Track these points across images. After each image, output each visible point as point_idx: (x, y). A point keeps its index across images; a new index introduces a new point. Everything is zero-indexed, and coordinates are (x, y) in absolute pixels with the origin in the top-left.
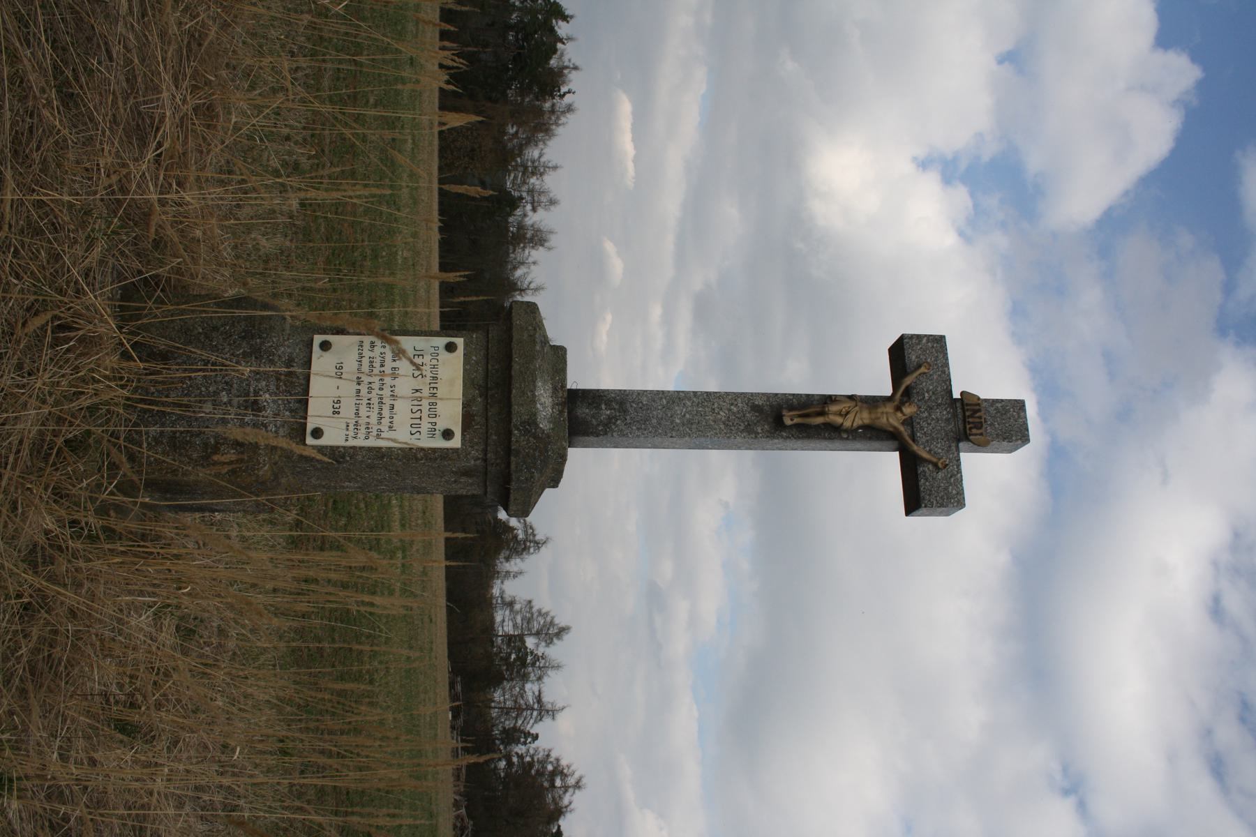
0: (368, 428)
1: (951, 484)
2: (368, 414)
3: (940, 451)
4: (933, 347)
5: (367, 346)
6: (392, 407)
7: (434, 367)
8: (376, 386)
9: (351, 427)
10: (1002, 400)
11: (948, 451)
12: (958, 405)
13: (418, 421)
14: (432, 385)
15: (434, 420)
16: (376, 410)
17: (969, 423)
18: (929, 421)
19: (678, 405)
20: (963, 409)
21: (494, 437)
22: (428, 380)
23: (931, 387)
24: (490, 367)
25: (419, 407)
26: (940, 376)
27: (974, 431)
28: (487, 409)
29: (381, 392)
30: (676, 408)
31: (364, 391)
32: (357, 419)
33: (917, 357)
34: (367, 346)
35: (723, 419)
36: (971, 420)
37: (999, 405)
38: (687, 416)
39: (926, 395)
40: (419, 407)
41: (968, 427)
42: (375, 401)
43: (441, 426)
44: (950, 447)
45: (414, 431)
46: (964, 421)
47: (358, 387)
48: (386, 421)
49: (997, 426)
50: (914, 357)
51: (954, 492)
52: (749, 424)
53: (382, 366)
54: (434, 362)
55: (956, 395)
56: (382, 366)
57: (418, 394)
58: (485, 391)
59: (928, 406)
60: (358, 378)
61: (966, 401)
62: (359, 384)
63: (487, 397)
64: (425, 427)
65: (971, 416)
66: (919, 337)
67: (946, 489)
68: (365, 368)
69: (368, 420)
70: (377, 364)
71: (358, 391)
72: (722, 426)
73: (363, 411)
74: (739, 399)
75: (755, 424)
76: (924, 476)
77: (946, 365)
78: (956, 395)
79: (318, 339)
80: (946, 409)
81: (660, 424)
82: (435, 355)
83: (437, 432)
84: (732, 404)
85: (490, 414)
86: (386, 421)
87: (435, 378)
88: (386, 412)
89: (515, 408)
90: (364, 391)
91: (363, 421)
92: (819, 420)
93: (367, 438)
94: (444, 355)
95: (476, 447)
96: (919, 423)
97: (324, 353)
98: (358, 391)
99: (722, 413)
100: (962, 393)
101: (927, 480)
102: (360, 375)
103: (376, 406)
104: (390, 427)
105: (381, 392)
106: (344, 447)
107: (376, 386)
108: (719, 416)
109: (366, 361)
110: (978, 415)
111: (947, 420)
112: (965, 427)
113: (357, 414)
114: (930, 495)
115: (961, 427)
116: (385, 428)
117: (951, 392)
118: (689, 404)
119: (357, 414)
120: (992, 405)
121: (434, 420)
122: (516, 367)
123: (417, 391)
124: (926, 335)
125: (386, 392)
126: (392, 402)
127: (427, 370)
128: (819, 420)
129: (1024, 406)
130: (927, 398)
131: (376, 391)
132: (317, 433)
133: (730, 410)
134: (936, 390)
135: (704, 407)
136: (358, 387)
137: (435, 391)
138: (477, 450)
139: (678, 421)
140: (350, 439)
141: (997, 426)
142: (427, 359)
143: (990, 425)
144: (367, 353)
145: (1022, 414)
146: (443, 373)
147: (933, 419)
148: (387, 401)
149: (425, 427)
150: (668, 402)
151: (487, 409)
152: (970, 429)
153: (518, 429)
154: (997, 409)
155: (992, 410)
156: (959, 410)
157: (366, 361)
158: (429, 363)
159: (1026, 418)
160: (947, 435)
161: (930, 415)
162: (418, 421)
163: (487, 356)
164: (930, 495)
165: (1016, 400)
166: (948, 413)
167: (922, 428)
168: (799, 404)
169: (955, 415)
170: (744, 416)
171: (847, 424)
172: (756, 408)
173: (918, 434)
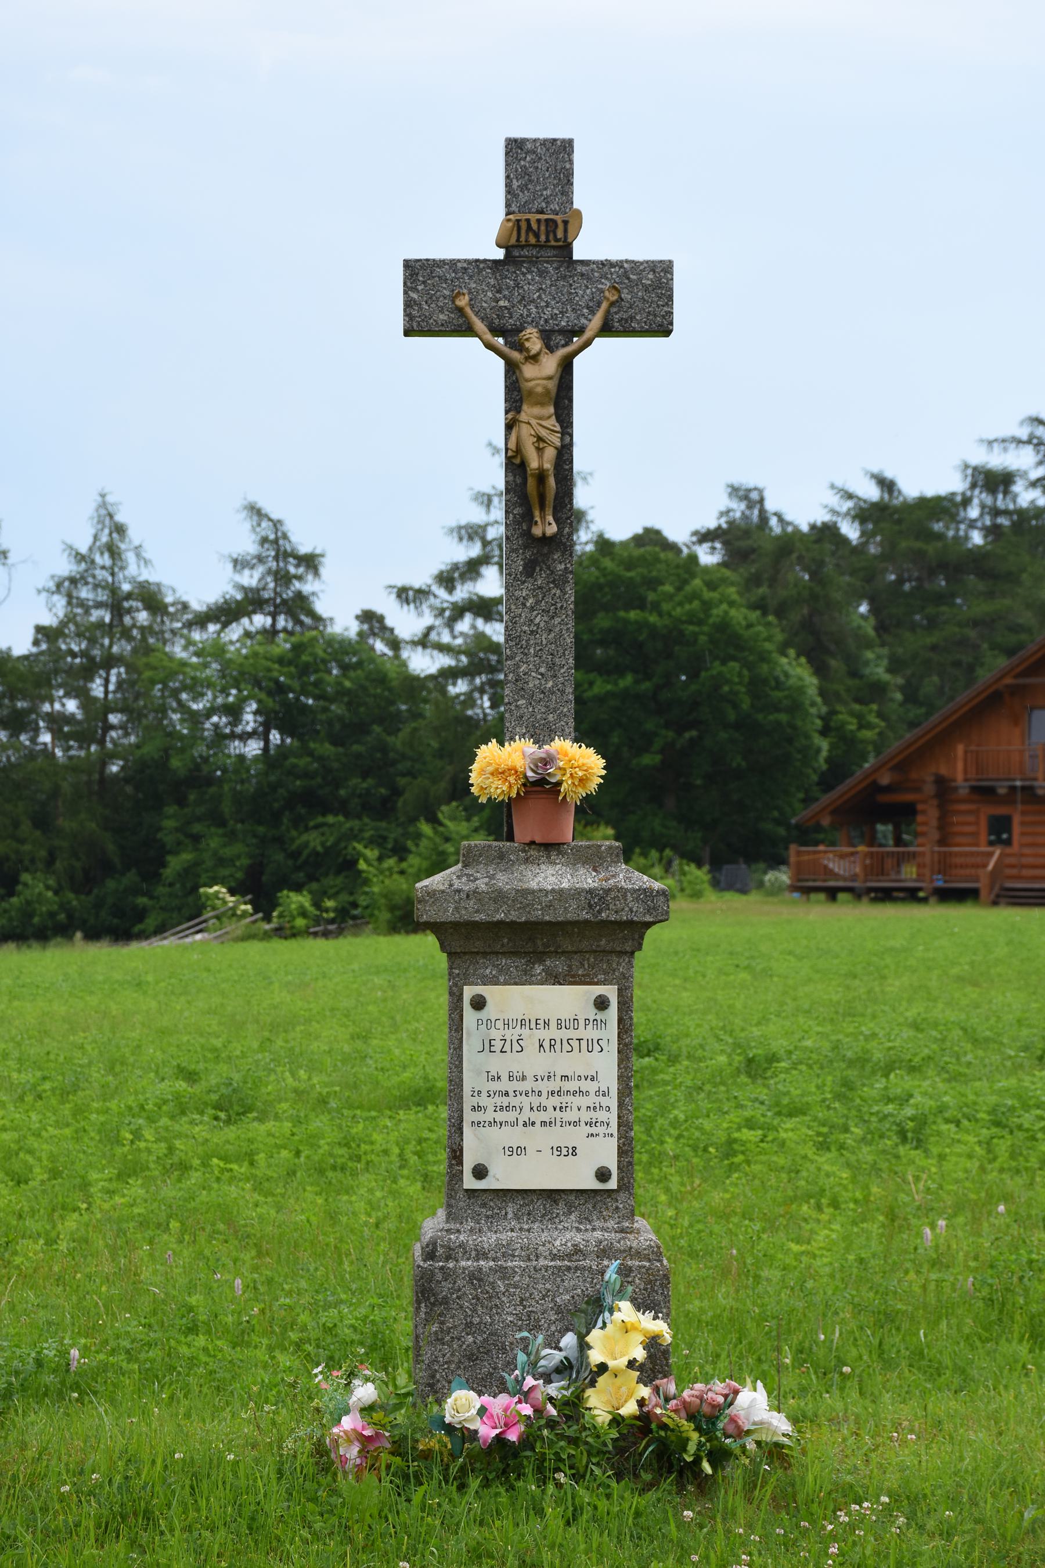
0: (595, 1108)
1: (640, 280)
2: (575, 1109)
3: (588, 291)
4: (424, 282)
5: (478, 1116)
6: (565, 1077)
7: (507, 1024)
8: (535, 1101)
9: (594, 1130)
10: (508, 177)
11: (589, 279)
12: (516, 253)
13: (584, 1043)
14: (533, 1026)
15: (582, 1022)
16: (570, 1099)
17: (547, 240)
18: (543, 304)
19: (527, 683)
20: (522, 247)
21: (603, 942)
22: (526, 1032)
23: (489, 294)
24: (505, 949)
25: (565, 1042)
26: (471, 277)
27: (560, 234)
28: (563, 952)
29: (545, 1094)
30: (531, 685)
31: (539, 1117)
32: (583, 1124)
33: (442, 312)
34: (478, 1116)
35: (545, 618)
36: (543, 238)
37: (515, 184)
38: (542, 670)
39: (502, 303)
40: (565, 1042)
41: (553, 243)
42: (555, 1101)
43: (592, 1013)
44: (582, 275)
45: (597, 1048)
46: (541, 247)
47: (538, 1124)
48: (585, 1085)
49: (549, 192)
50: (441, 317)
51: (651, 276)
52: (553, 582)
53: (507, 1094)
54: (499, 1024)
55: (499, 254)
56: (507, 1094)
57: (546, 1045)
58: (539, 956)
59: (520, 302)
60: (525, 1124)
61: (513, 241)
62: (533, 1124)
63: (544, 953)
64: (592, 1033)
65: (537, 235)
66: (408, 304)
67: (646, 289)
68: (511, 1116)
69: (583, 1109)
70: (505, 1101)
71: (544, 1123)
72: (557, 620)
73: (570, 1116)
74: (517, 593)
75: (552, 572)
76: (626, 321)
77: (452, 264)
78: (499, 254)
79: (470, 1182)
80: (524, 274)
81: (555, 710)
82: (490, 1023)
83: (598, 1017)
84: (524, 604)
85: (570, 948)
86: (585, 1085)
87: (522, 1023)
88: (572, 1086)
89: (570, 916)
90: (539, 1117)
91: (586, 1116)
92: (552, 482)
93: (608, 1109)
94: (491, 1011)
95: (614, 965)
96: (546, 321)
97: (491, 1173)
98: (544, 1123)
99: (537, 620)
100: (499, 245)
101: (632, 318)
102: (521, 1123)
103: (565, 1099)
104: (592, 1079)
105: (545, 1094)
106: (619, 1139)
107: (535, 1101)
108: (542, 624)
109: (500, 1116)
110: (535, 226)
111: (542, 273)
112: (554, 247)
113: (576, 1124)
114: (655, 316)
115: (550, 253)
116: (591, 1087)
117: (495, 262)
118: (524, 667)
119: (576, 1124)
120: (516, 196)
121: (582, 1022)
122: (513, 916)
123: (541, 1046)
124: (405, 293)
125: (545, 1086)
126: (558, 1078)
127: (512, 1034)
128: (552, 482)
129: (516, 140)
130: (506, 304)
131: (543, 1100)
132: (603, 1175)
133: (532, 609)
134: (494, 286)
135: (528, 646)
136: (538, 1124)
137: (541, 1022)
138: (619, 964)
139: (550, 684)
140: (610, 1131)
141: (549, 192)
142: (495, 1034)
143: (547, 203)
144: (489, 1116)
145: (529, 146)
146: (515, 1013)
147: (539, 297)
148: (554, 1085)
149: (592, 1033)
150: (523, 697)
151: (563, 952)
152: (557, 240)
153: (600, 912)
154: (523, 188)
155: (523, 197)
156: (525, 252)
157: (500, 1116)
158: (501, 1032)
159: (535, 140)
160: (564, 278)
161: (533, 301)
162: (584, 1043)
163: (485, 954)
164: (655, 316)
165: (507, 154)
166: (530, 272)
167: (554, 317)
168: (521, 505)
169: (533, 261)
170: (540, 588)
171: (556, 440)
172: (530, 569)
173: (563, 323)
